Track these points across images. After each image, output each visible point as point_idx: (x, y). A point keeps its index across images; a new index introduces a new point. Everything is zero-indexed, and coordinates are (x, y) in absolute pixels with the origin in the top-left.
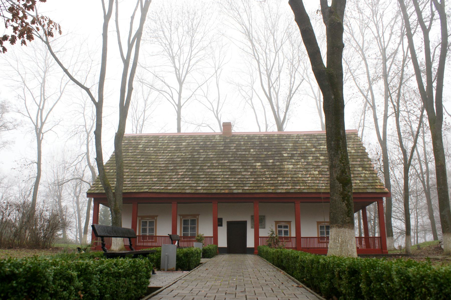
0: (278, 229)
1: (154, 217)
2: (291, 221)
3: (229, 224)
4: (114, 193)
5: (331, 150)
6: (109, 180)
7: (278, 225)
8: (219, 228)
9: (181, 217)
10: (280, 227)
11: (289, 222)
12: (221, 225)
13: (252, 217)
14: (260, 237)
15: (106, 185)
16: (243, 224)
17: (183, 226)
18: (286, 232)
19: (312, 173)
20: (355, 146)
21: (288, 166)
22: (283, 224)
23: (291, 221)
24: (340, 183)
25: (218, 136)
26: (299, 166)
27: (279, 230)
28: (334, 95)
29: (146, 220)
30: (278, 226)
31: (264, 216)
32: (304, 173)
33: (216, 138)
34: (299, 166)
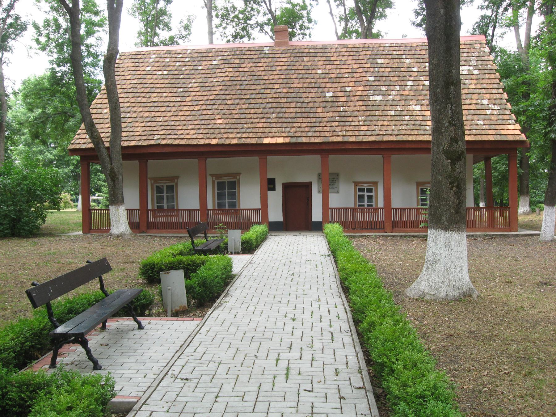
0: (358, 193)
1: (174, 179)
2: (378, 182)
3: (287, 187)
4: (108, 148)
5: (436, 102)
6: (100, 131)
7: (358, 187)
8: (270, 194)
9: (214, 178)
10: (361, 190)
11: (375, 184)
12: (273, 189)
13: (320, 177)
14: (331, 209)
15: (94, 138)
16: (307, 186)
17: (216, 191)
18: (370, 198)
19: (411, 109)
20: (480, 63)
21: (375, 98)
22: (366, 186)
23: (378, 182)
24: (447, 159)
25: (268, 48)
26: (391, 97)
27: (359, 195)
28: (446, 8)
29: (162, 184)
30: (359, 189)
31: (338, 175)
32: (399, 109)
33: (264, 52)
34: (391, 97)
